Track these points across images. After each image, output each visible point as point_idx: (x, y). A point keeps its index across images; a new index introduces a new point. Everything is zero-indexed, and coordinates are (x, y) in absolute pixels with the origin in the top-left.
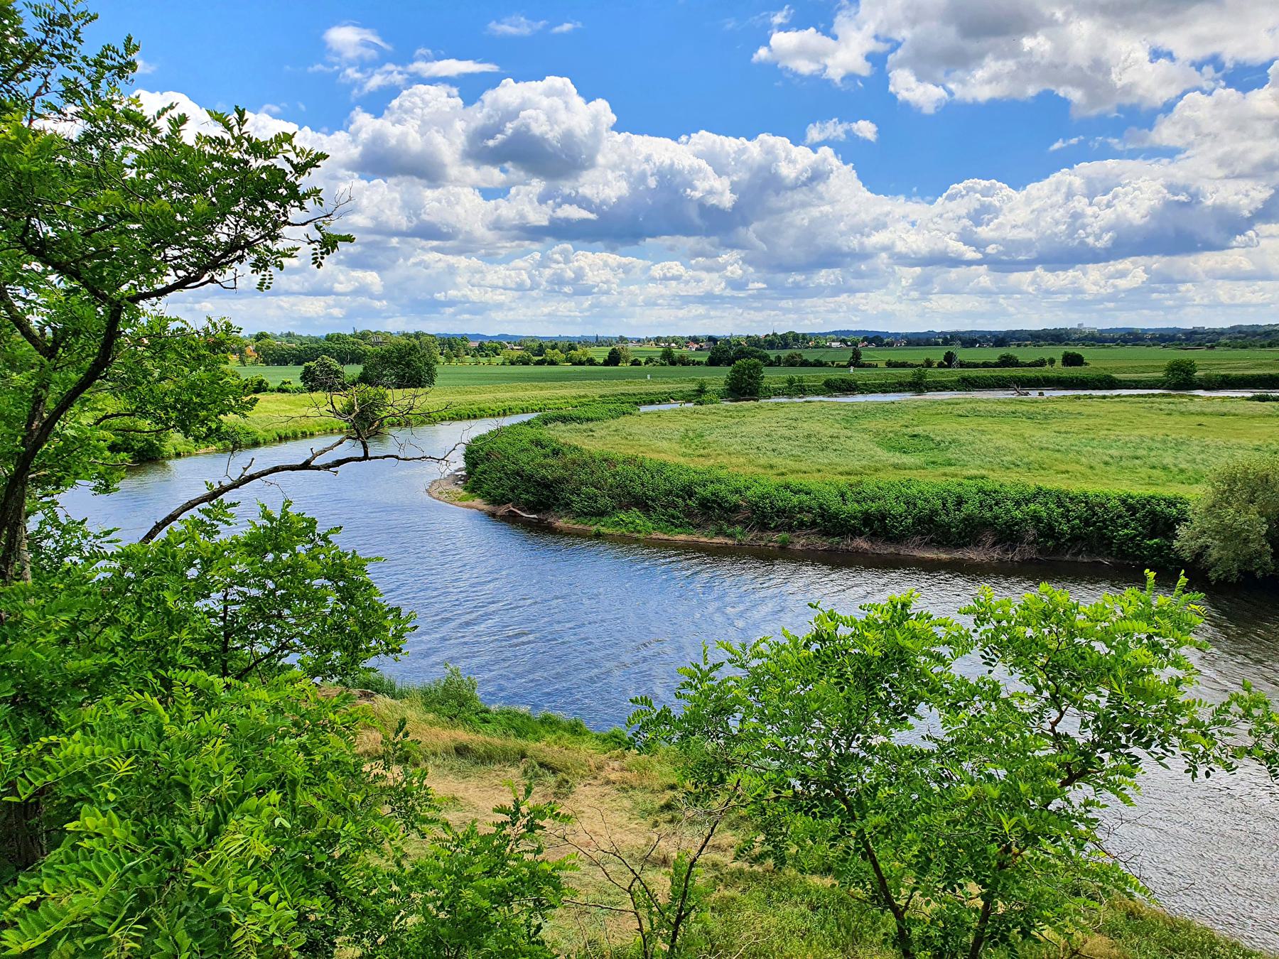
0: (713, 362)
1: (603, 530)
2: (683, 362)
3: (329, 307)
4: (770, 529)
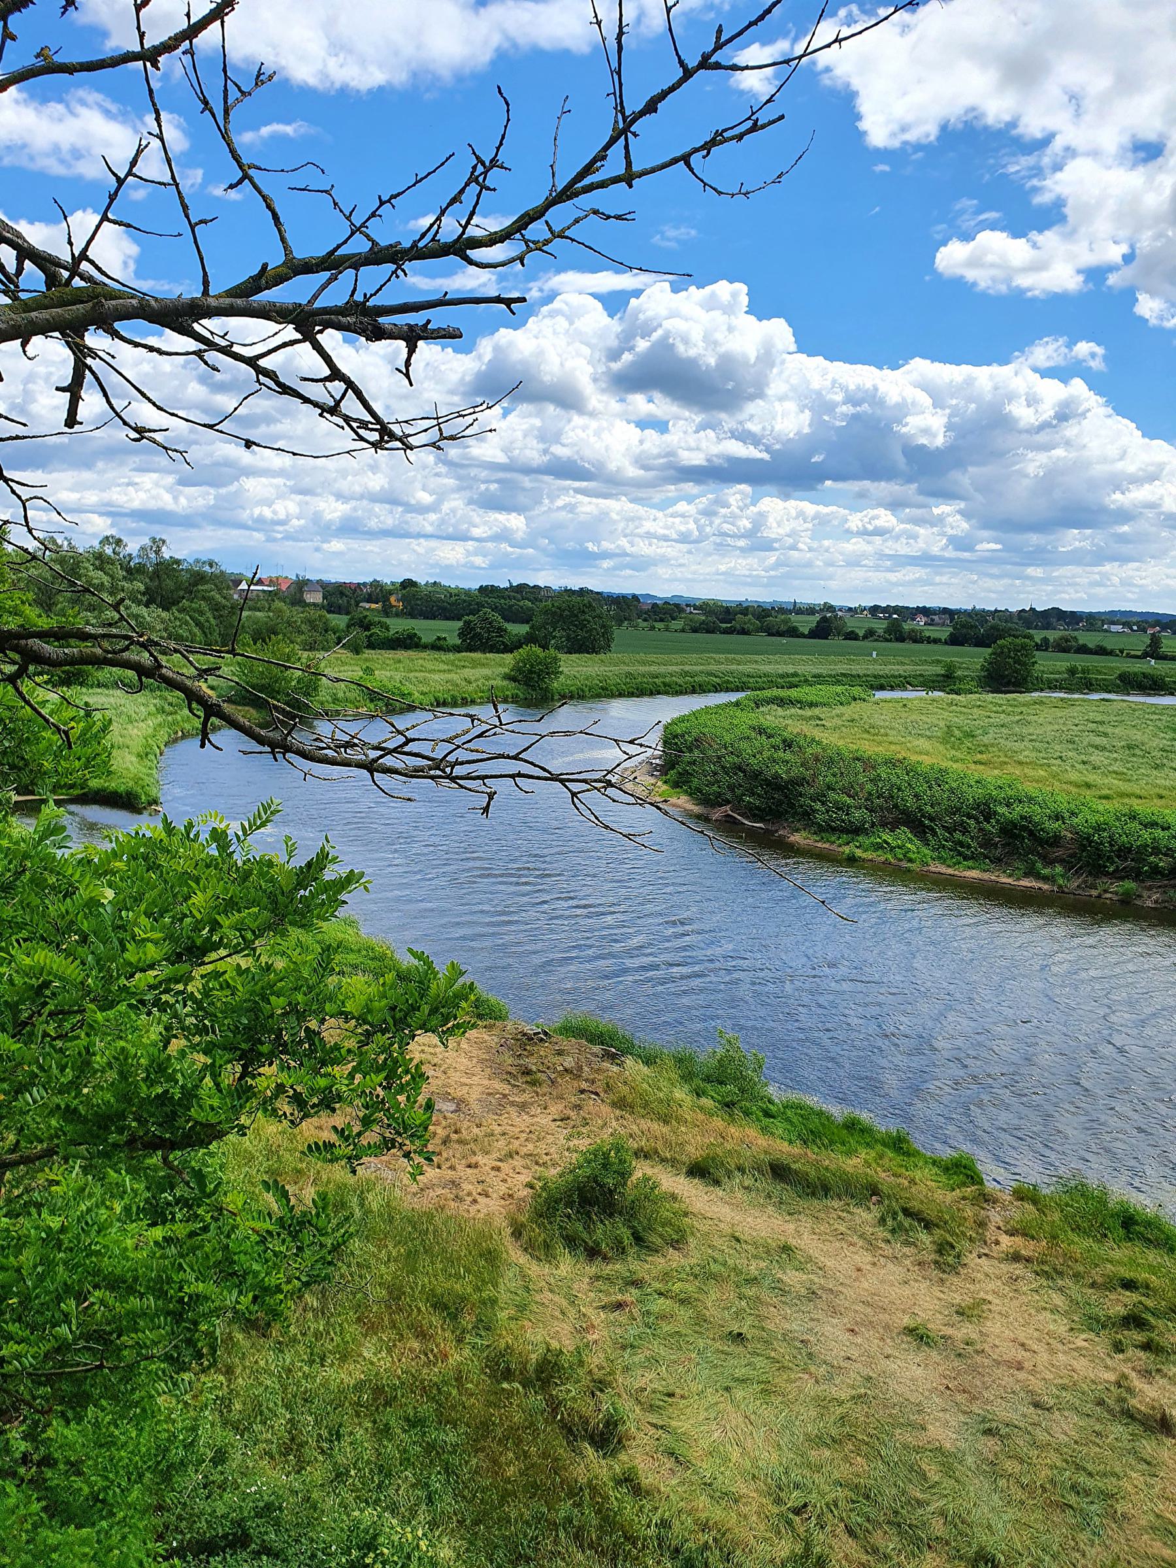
0: (954, 640)
1: (859, 853)
2: (916, 638)
3: (468, 553)
4: (1107, 874)
